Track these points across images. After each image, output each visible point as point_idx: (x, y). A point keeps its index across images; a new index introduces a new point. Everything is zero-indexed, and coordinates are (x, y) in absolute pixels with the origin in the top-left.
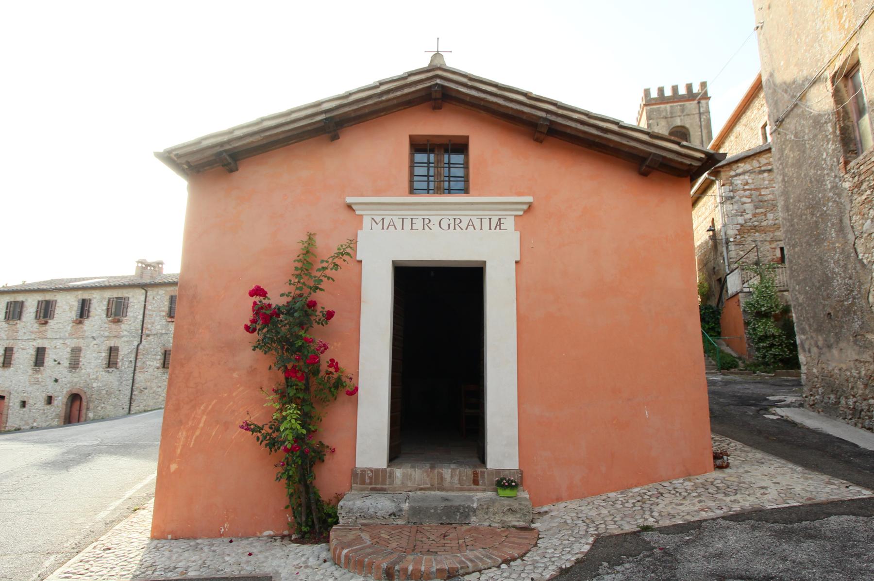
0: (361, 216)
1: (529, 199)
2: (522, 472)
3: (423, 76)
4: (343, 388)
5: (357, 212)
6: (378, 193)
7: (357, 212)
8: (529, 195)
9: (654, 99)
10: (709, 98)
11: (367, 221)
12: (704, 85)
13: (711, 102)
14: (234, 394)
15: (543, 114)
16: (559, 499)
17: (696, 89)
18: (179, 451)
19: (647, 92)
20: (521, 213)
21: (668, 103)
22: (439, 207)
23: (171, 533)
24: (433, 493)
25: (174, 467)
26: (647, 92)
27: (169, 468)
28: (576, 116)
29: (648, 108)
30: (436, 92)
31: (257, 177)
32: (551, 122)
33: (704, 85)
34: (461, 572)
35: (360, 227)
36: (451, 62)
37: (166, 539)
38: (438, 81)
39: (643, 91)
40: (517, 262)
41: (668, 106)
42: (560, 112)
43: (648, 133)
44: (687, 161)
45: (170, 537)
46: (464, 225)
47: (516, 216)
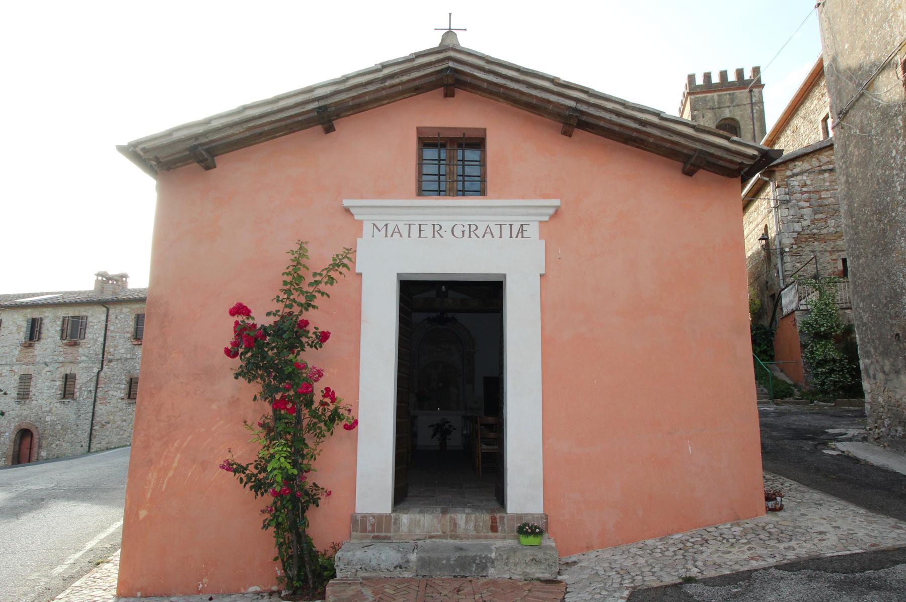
5: (356, 217)
7: (356, 217)
9: (699, 86)
10: (763, 86)
12: (756, 70)
13: (764, 91)
14: (214, 429)
16: (589, 548)
17: (747, 75)
18: (149, 496)
19: (691, 78)
20: (546, 218)
21: (715, 91)
23: (141, 589)
24: (444, 541)
25: (143, 514)
26: (691, 78)
27: (137, 514)
28: (610, 106)
29: (693, 97)
30: (448, 74)
31: (235, 171)
33: (756, 70)
37: (135, 597)
39: (686, 77)
41: (715, 94)
42: (592, 100)
43: (693, 127)
45: (139, 594)
46: (480, 232)
47: (540, 222)
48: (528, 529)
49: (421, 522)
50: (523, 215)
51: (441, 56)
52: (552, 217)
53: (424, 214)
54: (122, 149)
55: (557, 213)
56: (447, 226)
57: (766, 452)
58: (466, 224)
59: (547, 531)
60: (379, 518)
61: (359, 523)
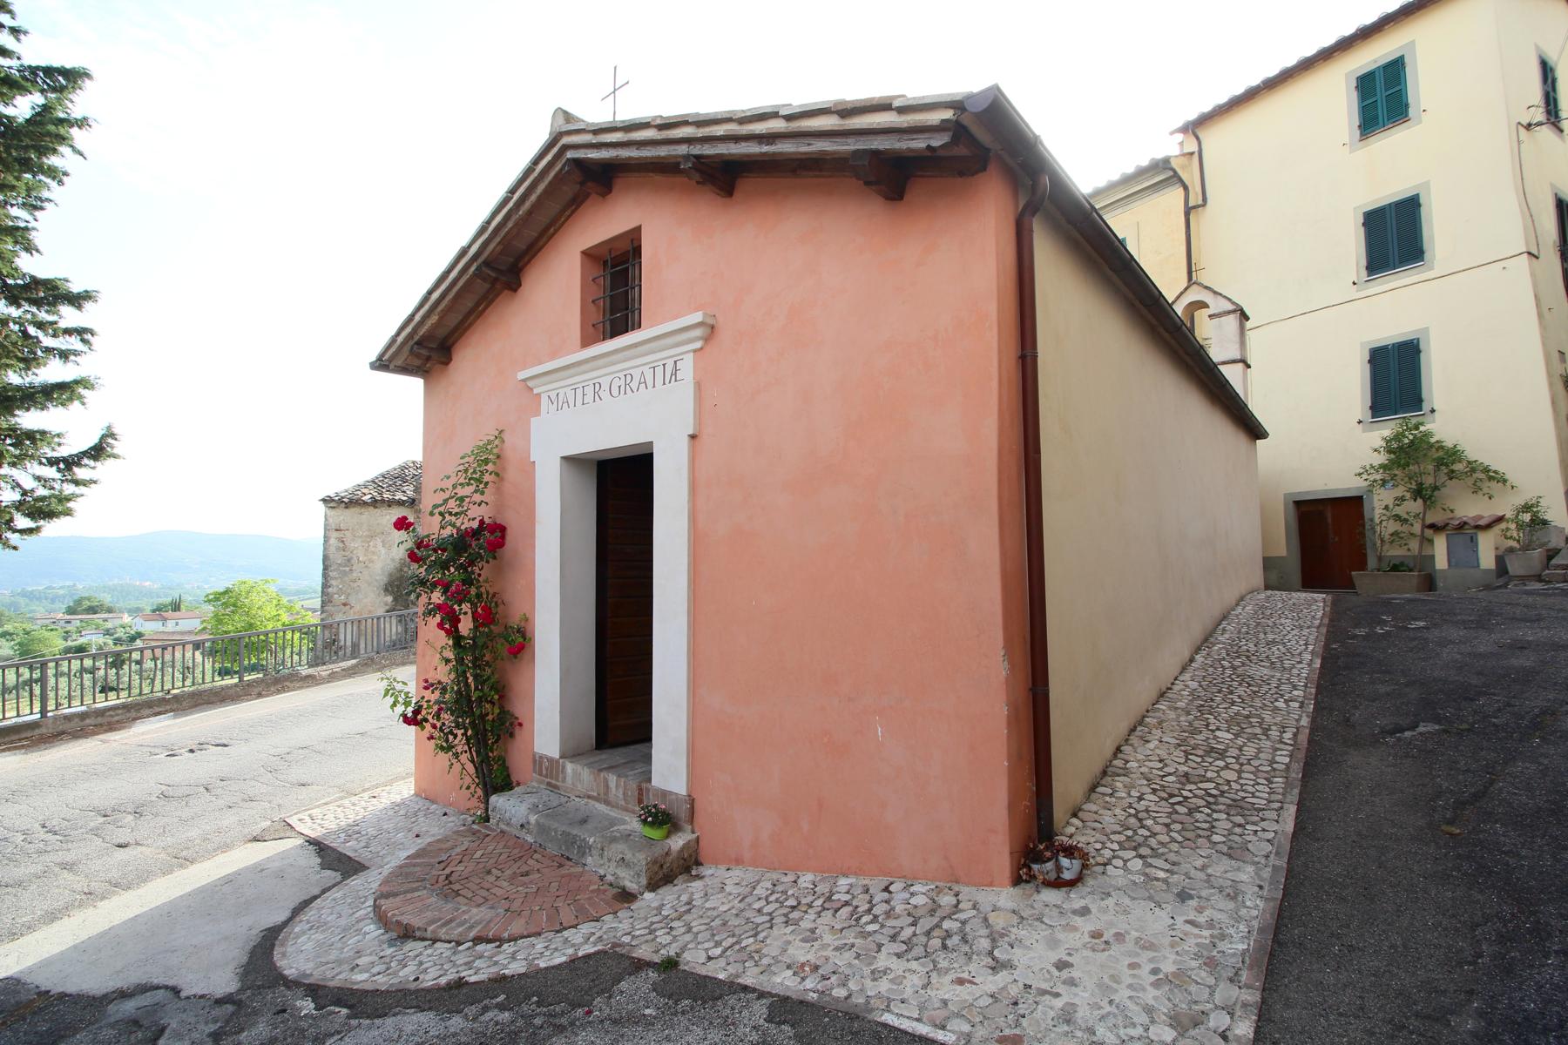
0: (539, 395)
1: (697, 317)
2: (692, 801)
3: (549, 157)
4: (520, 644)
6: (553, 356)
8: (696, 310)
11: (544, 399)
15: (682, 150)
16: (738, 861)
20: (698, 345)
22: (620, 356)
24: (597, 805)
28: (719, 130)
30: (580, 171)
32: (698, 157)
34: (418, 934)
35: (537, 413)
36: (595, 112)
38: (570, 154)
40: (693, 437)
44: (919, 144)
47: (695, 351)
48: (662, 818)
49: (578, 775)
50: (605, 366)
51: (555, 150)
52: (706, 340)
53: (613, 364)
54: (383, 364)
55: (710, 331)
56: (605, 381)
57: (1419, 352)
58: (621, 375)
59: (691, 820)
60: (551, 760)
61: (538, 761)
